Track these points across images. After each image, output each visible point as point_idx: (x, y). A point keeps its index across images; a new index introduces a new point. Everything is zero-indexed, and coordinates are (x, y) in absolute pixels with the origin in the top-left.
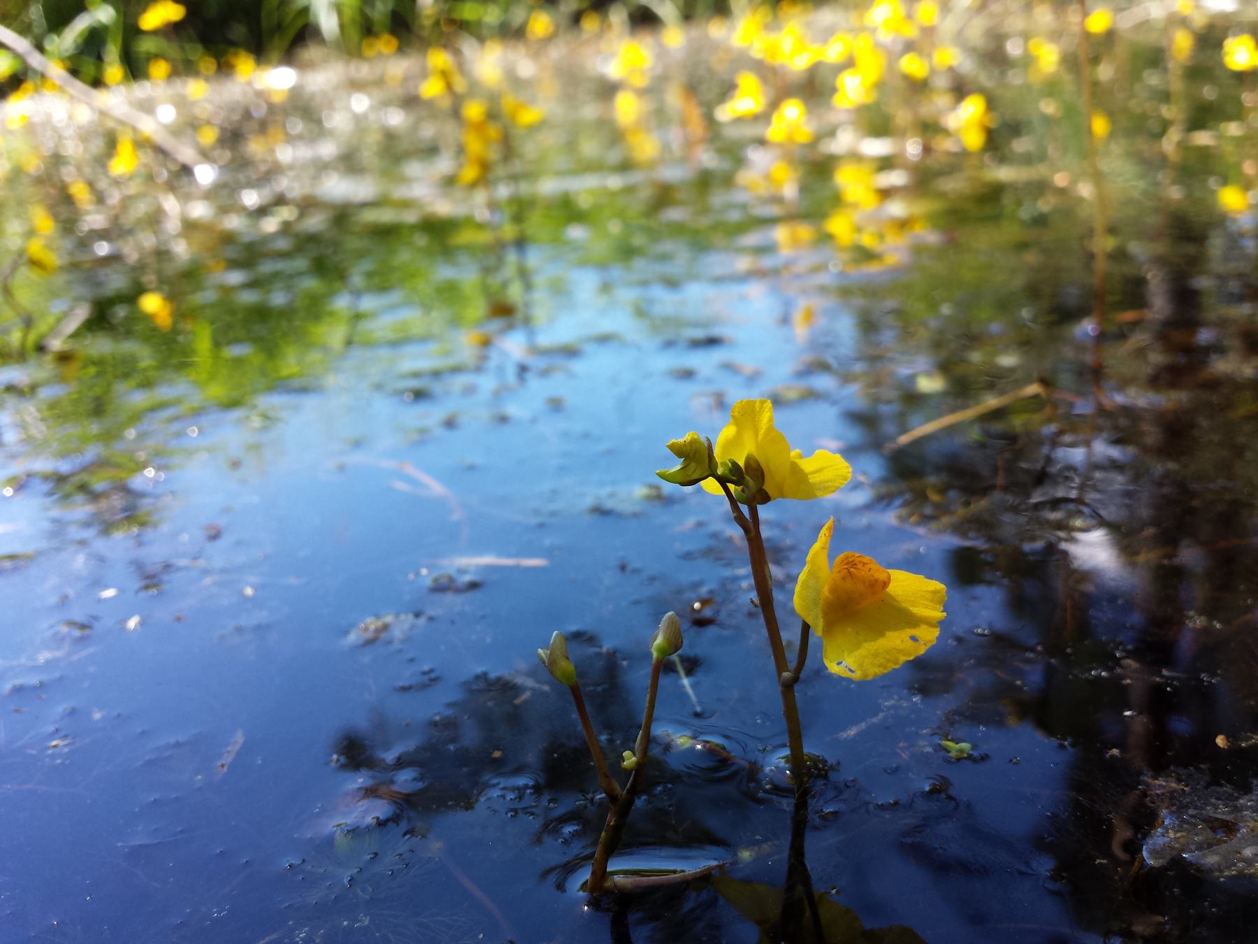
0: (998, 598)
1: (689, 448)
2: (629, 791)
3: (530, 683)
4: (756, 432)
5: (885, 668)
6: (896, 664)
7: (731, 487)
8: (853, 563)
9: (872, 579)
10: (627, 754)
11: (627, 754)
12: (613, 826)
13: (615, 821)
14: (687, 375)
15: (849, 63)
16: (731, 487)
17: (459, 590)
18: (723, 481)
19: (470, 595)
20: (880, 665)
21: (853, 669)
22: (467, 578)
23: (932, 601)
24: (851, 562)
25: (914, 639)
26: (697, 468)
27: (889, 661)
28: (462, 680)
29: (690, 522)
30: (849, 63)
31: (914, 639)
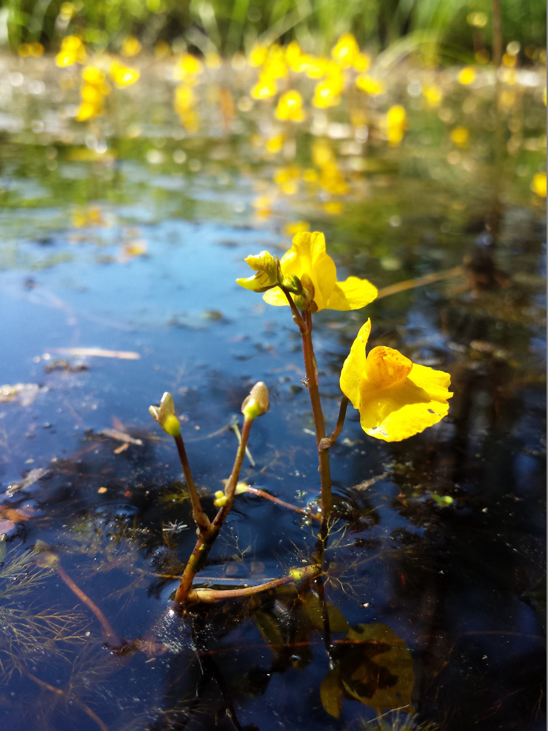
0: (158, 450)
1: (263, 263)
2: (216, 524)
3: (126, 438)
4: (310, 258)
5: (411, 432)
6: (419, 429)
7: (292, 295)
8: (384, 354)
9: (400, 365)
10: (218, 494)
11: (218, 494)
12: (201, 551)
13: (204, 546)
14: (231, 245)
15: (324, 78)
16: (292, 295)
17: (73, 371)
18: (286, 290)
19: (84, 374)
20: (408, 430)
21: (386, 433)
22: (79, 363)
23: (440, 385)
24: (383, 353)
25: (430, 411)
26: (268, 278)
27: (414, 427)
28: (254, 278)
29: (240, 336)
30: (324, 78)
31: (430, 411)
